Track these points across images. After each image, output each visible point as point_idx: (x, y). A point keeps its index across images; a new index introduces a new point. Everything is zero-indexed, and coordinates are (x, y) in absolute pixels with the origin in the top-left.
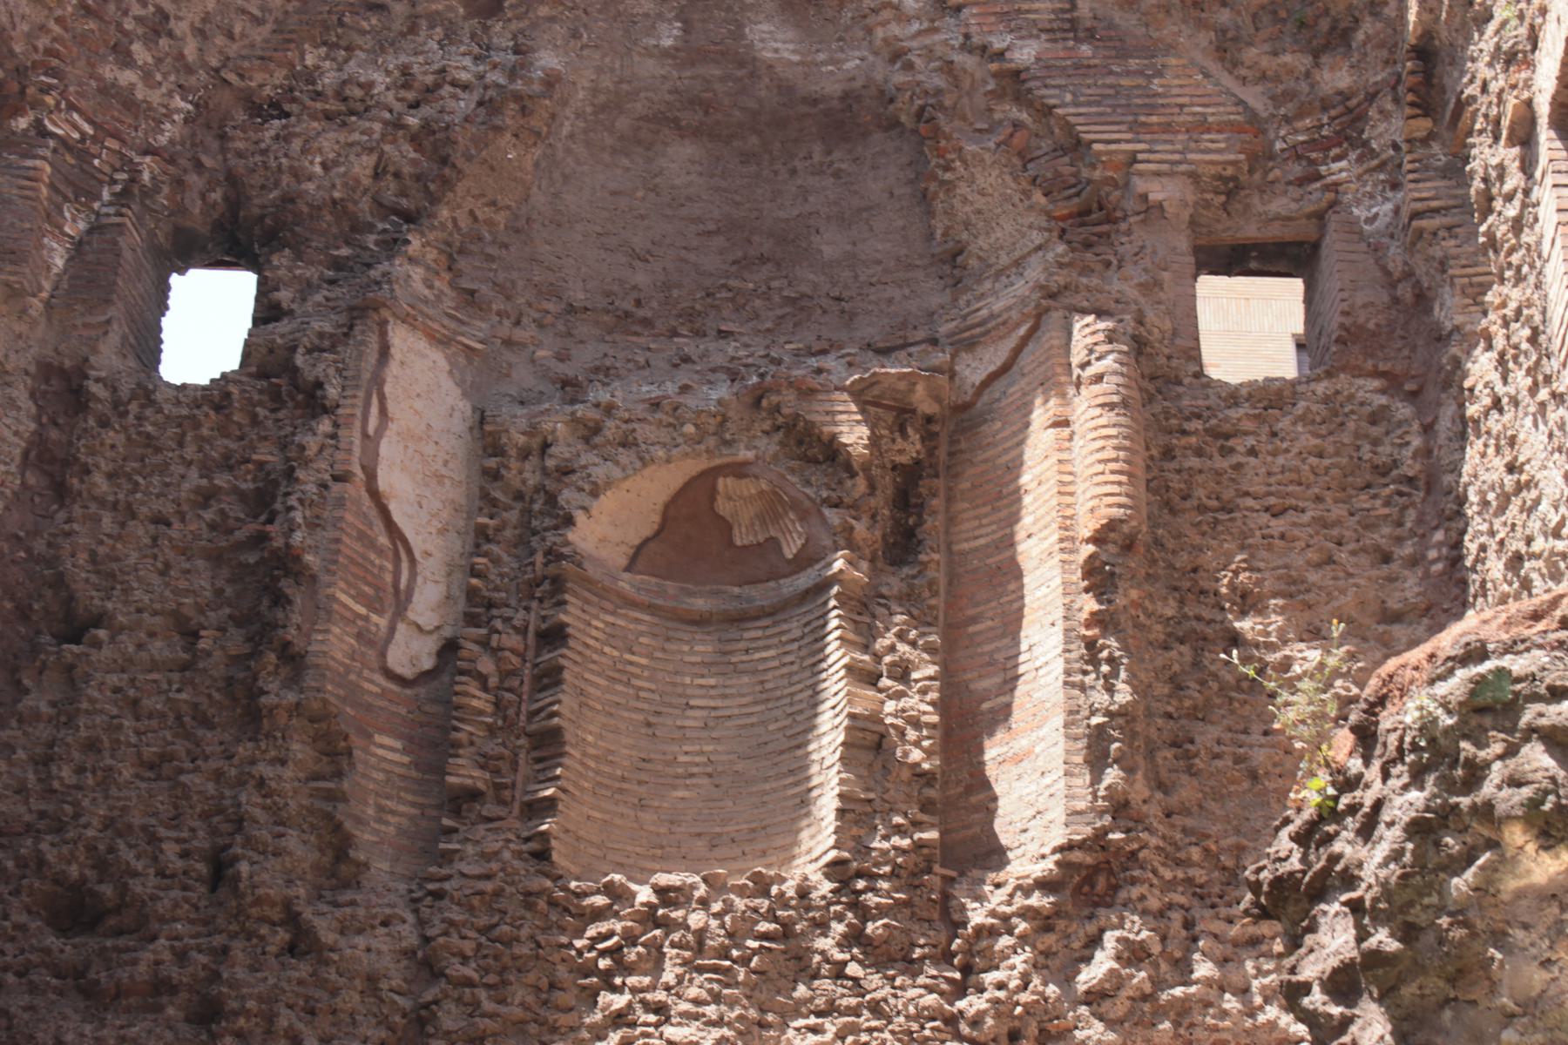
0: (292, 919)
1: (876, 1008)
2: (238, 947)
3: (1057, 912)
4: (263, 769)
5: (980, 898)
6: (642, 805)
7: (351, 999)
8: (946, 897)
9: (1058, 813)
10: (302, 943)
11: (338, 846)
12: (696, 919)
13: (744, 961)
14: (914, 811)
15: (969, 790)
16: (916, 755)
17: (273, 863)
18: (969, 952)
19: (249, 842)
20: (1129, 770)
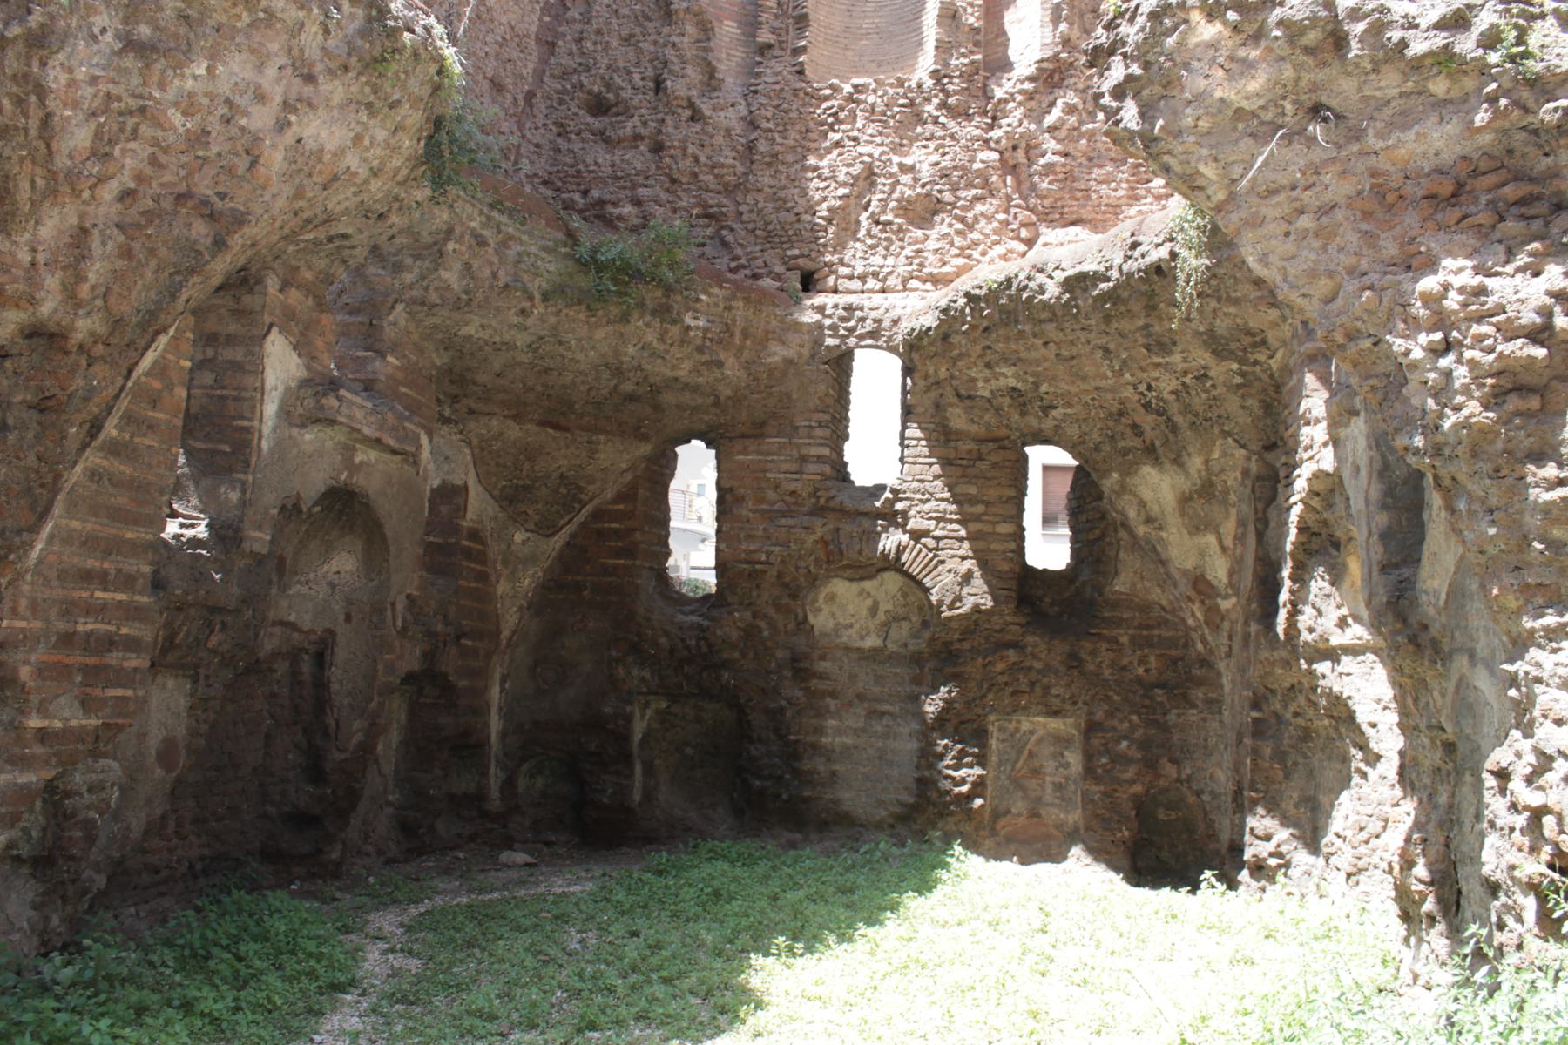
0: (691, 105)
1: (952, 137)
2: (669, 118)
3: (1036, 91)
4: (674, 39)
5: (1000, 85)
6: (846, 48)
7: (719, 139)
8: (985, 85)
9: (1037, 44)
10: (697, 116)
11: (711, 72)
12: (871, 99)
13: (893, 117)
14: (970, 46)
15: (997, 36)
16: (971, 20)
17: (681, 80)
18: (995, 110)
19: (670, 72)
20: (1071, 24)
